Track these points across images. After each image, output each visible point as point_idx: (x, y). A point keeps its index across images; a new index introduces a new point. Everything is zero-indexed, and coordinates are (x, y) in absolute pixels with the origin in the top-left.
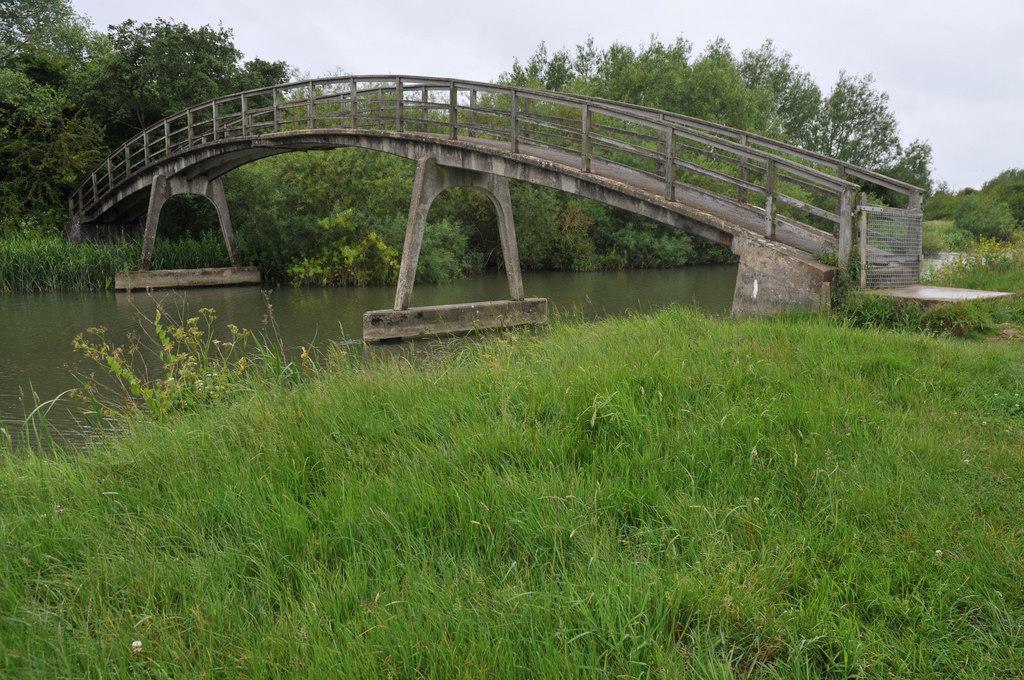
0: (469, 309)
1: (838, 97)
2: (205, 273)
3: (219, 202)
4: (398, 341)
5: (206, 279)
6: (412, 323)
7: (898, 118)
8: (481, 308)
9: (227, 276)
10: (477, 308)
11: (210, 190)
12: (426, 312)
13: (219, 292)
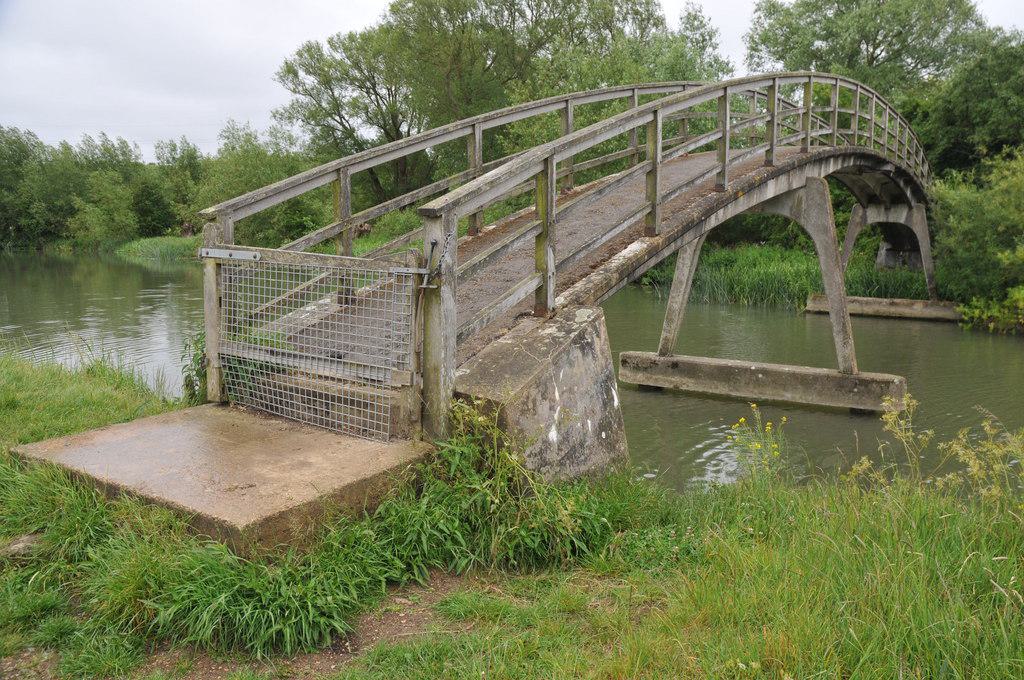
0: (746, 370)
1: (972, 7)
2: (892, 304)
3: (920, 230)
4: (658, 390)
5: (893, 310)
6: (665, 373)
7: (198, 145)
8: (765, 372)
9: (918, 309)
10: (758, 371)
11: (909, 217)
12: (684, 363)
13: (908, 325)
